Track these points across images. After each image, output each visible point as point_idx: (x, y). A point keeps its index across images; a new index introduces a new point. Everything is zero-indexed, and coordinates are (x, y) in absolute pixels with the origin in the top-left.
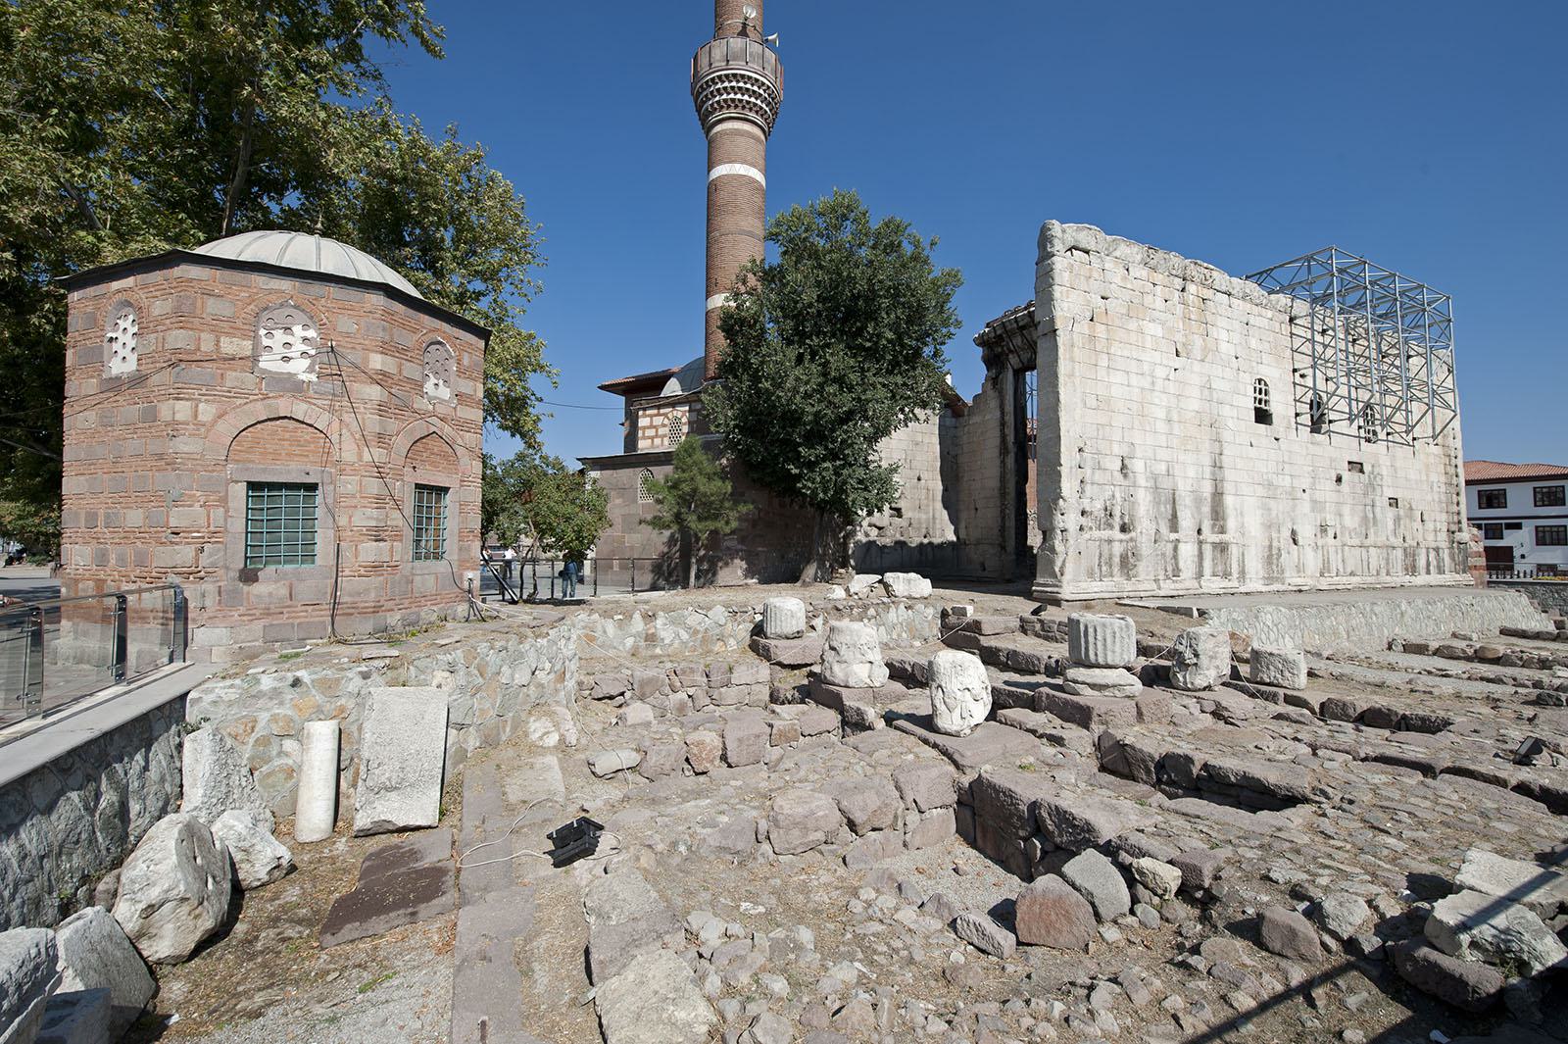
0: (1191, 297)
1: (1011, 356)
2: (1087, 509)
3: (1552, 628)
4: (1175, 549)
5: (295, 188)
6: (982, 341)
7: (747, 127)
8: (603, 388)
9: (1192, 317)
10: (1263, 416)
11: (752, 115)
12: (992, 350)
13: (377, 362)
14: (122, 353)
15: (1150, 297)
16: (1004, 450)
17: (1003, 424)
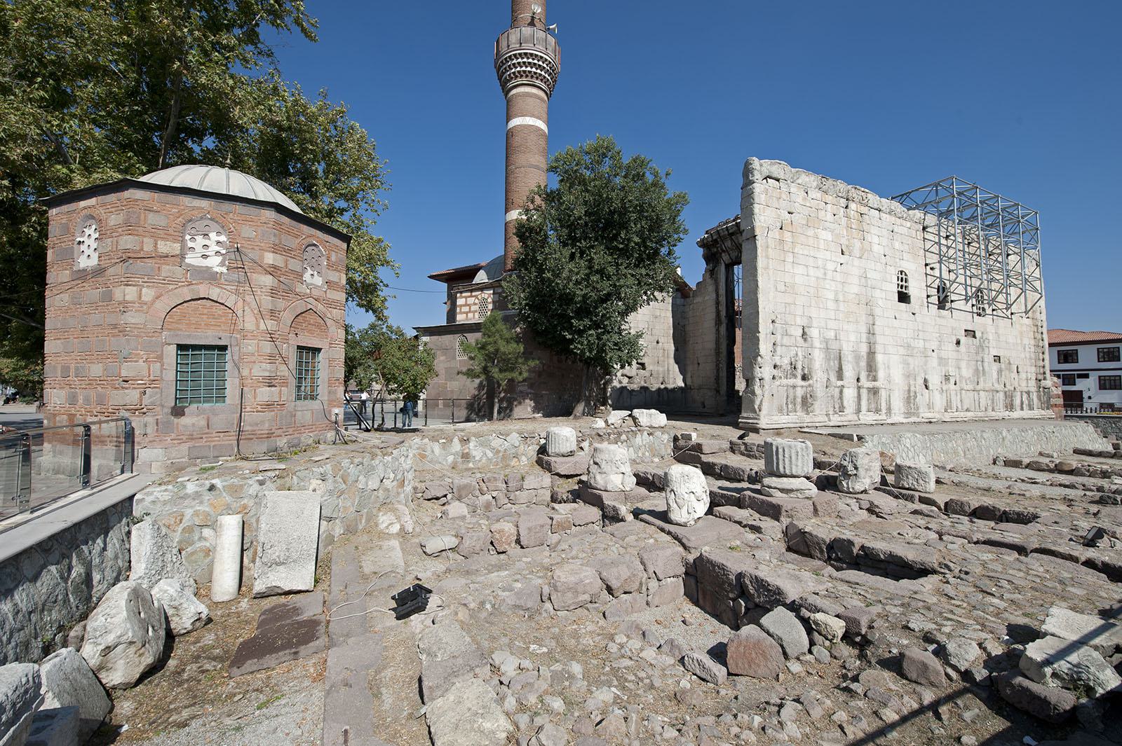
0: (852, 212)
1: (723, 254)
2: (778, 364)
3: (1110, 449)
4: (841, 392)
5: (211, 134)
6: (703, 244)
7: (534, 91)
8: (431, 277)
9: (853, 226)
10: (903, 297)
11: (538, 82)
12: (710, 250)
13: (270, 258)
14: (87, 252)
15: (823, 212)
16: (718, 321)
17: (718, 303)
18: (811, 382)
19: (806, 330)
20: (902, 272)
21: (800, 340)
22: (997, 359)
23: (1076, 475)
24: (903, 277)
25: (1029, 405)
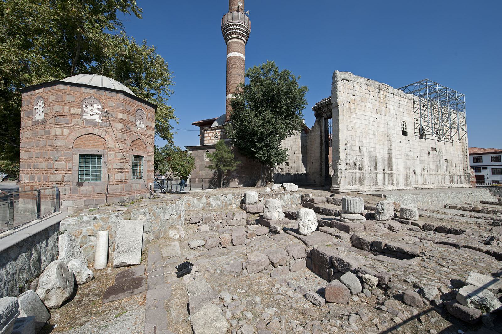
0: (381, 95)
1: (324, 114)
2: (348, 163)
3: (497, 201)
4: (376, 176)
5: (94, 60)
6: (314, 109)
7: (239, 41)
8: (193, 124)
9: (382, 101)
10: (404, 133)
11: (241, 37)
12: (318, 112)
13: (121, 116)
14: (39, 113)
15: (368, 95)
16: (321, 144)
17: (321, 136)
18: (363, 171)
19: (361, 148)
20: (403, 122)
21: (358, 152)
22: (446, 161)
23: (482, 213)
24: (404, 124)
25: (461, 181)
